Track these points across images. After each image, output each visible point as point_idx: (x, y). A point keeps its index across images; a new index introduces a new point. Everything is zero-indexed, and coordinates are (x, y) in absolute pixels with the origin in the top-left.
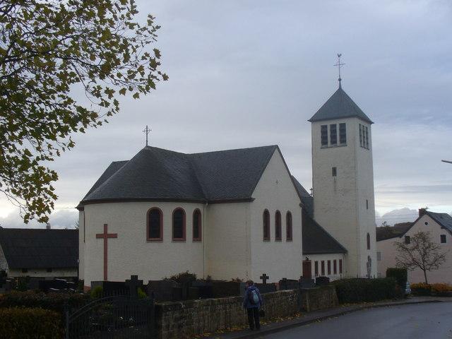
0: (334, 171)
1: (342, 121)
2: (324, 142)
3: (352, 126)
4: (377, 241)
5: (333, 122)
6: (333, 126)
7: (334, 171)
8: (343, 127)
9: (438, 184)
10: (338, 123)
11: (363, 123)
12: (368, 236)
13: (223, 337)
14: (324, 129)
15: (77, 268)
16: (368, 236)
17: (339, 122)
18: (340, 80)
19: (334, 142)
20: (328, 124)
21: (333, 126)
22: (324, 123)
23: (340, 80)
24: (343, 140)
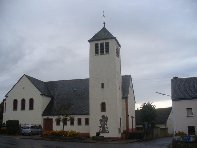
0: (103, 85)
1: (107, 41)
2: (97, 52)
3: (112, 44)
4: (71, 125)
5: (102, 42)
6: (102, 44)
7: (103, 85)
8: (107, 44)
9: (26, 129)
10: (104, 42)
11: (118, 46)
12: (121, 119)
13: (161, 147)
14: (96, 46)
15: (88, 114)
16: (121, 119)
17: (103, 43)
18: (104, 23)
19: (102, 52)
20: (99, 42)
21: (102, 44)
22: (96, 42)
23: (104, 23)
24: (107, 51)
